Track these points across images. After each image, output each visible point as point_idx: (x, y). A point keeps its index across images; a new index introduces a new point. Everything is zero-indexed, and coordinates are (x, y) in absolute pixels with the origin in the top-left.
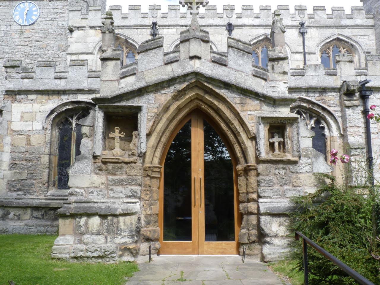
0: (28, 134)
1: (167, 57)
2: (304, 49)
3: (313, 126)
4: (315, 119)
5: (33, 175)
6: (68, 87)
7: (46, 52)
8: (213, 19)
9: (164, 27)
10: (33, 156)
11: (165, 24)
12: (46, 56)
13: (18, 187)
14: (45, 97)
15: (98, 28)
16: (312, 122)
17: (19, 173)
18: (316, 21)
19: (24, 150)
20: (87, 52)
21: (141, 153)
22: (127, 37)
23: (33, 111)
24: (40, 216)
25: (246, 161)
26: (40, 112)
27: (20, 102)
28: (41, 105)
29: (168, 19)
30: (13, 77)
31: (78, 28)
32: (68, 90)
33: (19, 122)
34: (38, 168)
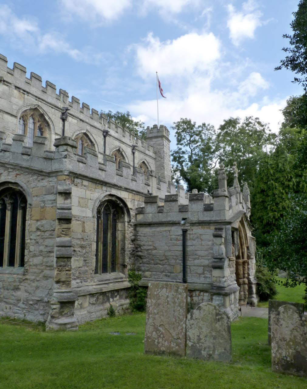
0: (83, 220)
5: (87, 261)
6: (106, 180)
10: (86, 243)
13: (77, 275)
14: (94, 185)
15: (22, 91)
17: (77, 260)
22: (45, 113)
23: (86, 197)
24: (94, 302)
26: (91, 199)
27: (77, 185)
30: (72, 157)
32: (109, 183)
33: (77, 207)
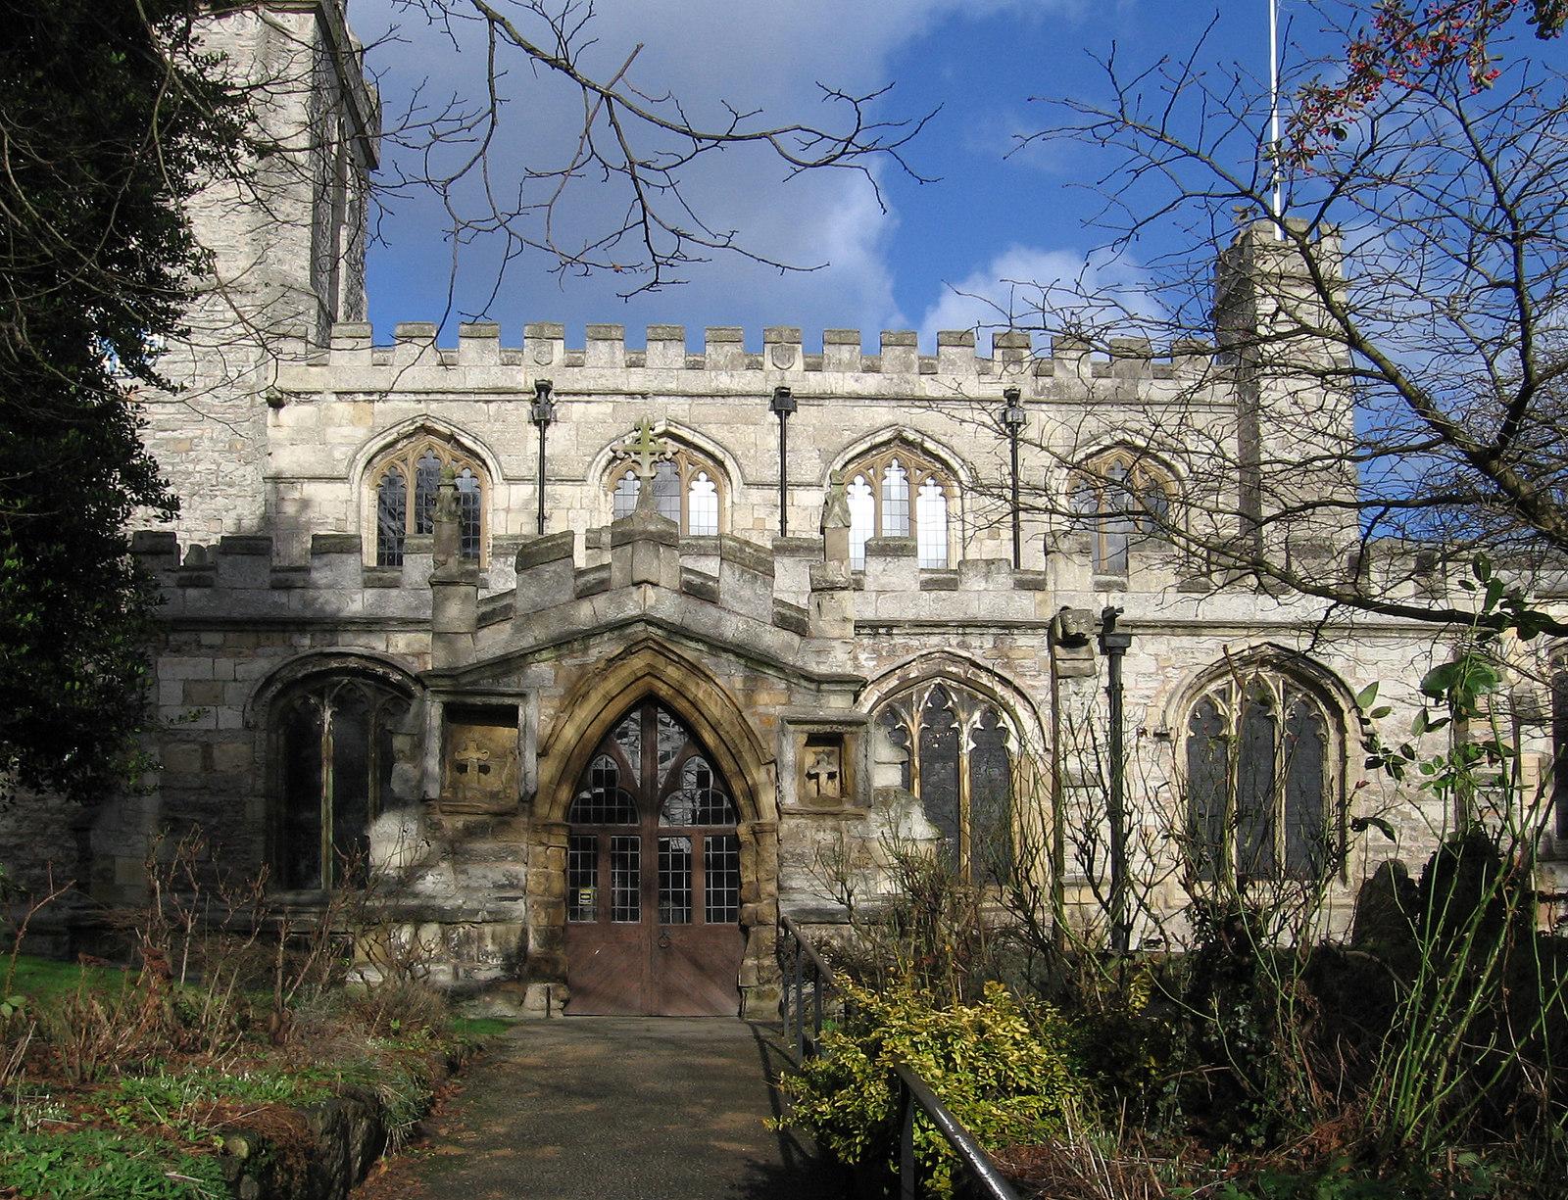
1: (582, 580)
2: (1014, 473)
3: (978, 725)
4: (983, 707)
7: (191, 467)
8: (732, 376)
9: (576, 398)
11: (577, 387)
12: (192, 480)
15: (362, 397)
16: (977, 716)
18: (1056, 386)
19: (197, 783)
20: (328, 473)
21: (527, 792)
25: (757, 813)
26: (235, 680)
27: (178, 651)
28: (237, 661)
29: (586, 371)
31: (297, 394)
34: (237, 833)
